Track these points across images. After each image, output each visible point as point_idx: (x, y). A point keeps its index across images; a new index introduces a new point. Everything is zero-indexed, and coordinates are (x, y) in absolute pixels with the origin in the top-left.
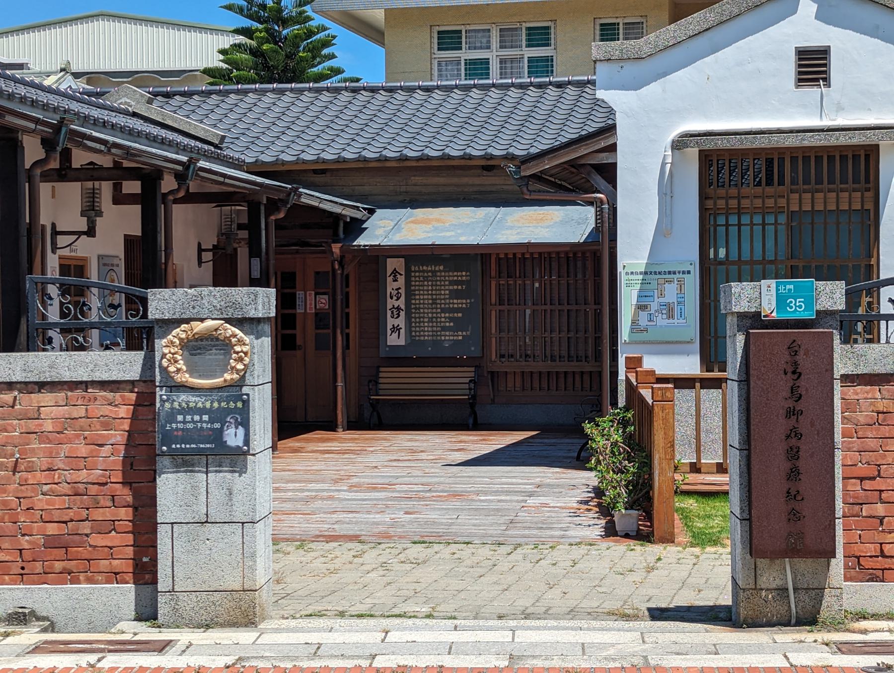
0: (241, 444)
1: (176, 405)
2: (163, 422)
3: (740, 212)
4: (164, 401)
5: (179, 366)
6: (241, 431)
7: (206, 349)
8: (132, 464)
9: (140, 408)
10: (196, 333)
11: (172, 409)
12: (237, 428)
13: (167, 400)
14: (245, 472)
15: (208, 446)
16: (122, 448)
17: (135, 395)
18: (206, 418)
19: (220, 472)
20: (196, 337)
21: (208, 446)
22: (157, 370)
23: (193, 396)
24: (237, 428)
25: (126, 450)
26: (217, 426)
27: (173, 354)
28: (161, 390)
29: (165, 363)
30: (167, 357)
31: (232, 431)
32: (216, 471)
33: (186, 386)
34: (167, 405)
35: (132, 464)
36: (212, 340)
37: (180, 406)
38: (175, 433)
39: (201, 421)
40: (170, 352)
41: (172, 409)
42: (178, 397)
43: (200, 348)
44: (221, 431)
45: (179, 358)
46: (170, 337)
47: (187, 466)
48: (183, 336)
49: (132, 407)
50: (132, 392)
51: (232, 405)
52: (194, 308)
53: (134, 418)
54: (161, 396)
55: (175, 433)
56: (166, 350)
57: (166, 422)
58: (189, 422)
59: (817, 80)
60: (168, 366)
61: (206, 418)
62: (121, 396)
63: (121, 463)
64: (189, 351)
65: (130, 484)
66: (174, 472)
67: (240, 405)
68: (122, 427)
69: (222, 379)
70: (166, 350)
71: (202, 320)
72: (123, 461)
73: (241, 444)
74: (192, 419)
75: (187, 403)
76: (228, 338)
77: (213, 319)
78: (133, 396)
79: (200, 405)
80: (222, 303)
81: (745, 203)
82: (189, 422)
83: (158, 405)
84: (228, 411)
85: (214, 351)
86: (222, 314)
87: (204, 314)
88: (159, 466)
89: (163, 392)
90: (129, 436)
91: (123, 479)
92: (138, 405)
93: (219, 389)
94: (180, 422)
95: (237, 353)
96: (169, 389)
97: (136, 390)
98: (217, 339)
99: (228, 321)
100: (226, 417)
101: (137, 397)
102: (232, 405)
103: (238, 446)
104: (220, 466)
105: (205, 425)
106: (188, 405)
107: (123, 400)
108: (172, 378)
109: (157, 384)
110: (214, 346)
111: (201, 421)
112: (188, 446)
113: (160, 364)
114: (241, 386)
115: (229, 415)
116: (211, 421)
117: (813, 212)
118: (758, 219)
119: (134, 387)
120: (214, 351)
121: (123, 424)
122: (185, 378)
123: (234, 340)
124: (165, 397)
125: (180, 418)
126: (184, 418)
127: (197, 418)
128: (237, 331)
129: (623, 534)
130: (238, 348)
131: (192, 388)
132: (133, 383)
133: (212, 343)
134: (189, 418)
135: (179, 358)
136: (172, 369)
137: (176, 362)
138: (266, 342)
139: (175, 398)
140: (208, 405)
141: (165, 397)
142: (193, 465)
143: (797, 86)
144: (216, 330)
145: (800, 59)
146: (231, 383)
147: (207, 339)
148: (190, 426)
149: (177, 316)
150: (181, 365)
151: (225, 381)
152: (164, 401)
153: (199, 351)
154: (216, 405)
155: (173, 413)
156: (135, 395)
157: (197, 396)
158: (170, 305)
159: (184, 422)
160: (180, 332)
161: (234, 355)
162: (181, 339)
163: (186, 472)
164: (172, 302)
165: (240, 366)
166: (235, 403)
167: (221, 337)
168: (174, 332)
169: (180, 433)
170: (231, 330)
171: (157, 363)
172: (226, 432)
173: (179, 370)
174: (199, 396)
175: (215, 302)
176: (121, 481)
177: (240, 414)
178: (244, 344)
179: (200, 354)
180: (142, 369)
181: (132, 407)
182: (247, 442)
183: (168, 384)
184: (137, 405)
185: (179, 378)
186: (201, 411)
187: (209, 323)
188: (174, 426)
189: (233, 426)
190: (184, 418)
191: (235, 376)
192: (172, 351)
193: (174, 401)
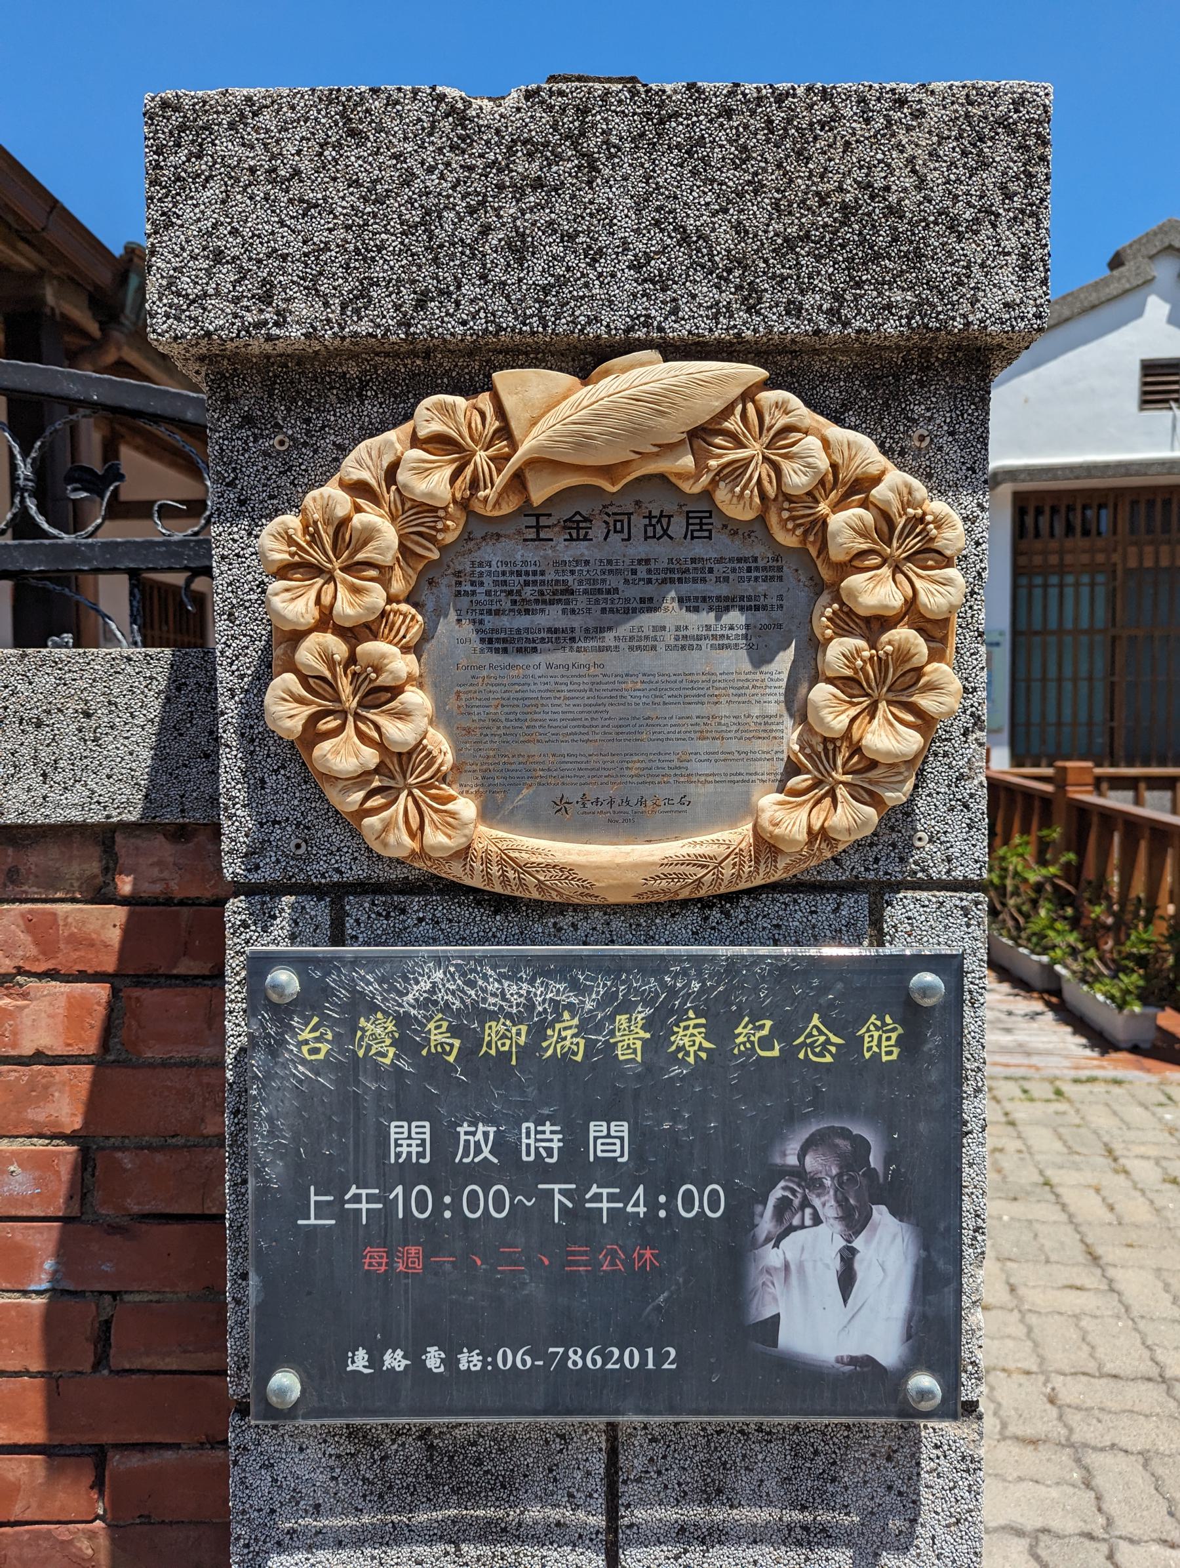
0: (887, 1347)
1: (377, 1036)
2: (275, 1172)
3: (1061, 570)
4: (282, 1012)
5: (399, 732)
6: (888, 1248)
7: (616, 600)
8: (103, 1336)
9: (150, 996)
10: (540, 463)
11: (348, 1067)
12: (855, 1221)
13: (311, 1000)
14: (904, 1543)
15: (631, 1358)
16: (42, 1241)
17: (119, 914)
18: (609, 1139)
19: (712, 1536)
20: (540, 491)
21: (631, 1358)
22: (230, 761)
23: (513, 968)
24: (855, 1221)
25: (64, 1252)
26: (701, 1202)
27: (353, 634)
28: (265, 919)
29: (286, 710)
30: (307, 654)
31: (816, 1245)
32: (683, 1534)
33: (454, 890)
34: (310, 1042)
35: (103, 1336)
36: (657, 527)
37: (402, 1044)
38: (374, 1259)
39: (575, 1163)
40: (326, 621)
41: (348, 1067)
42: (396, 976)
43: (562, 594)
44: (725, 1259)
45: (402, 665)
46: (329, 497)
47: (463, 1493)
48: (434, 482)
49: (100, 992)
50: (101, 895)
51: (819, 1040)
52: (519, 249)
53: (115, 1052)
54: (260, 965)
55: (374, 1259)
56: (294, 604)
57: (301, 1173)
58: (482, 1174)
59: (1166, 401)
60: (312, 735)
61: (609, 1139)
62: (30, 924)
63: (35, 1333)
64: (477, 614)
65: (99, 1455)
66: (359, 1539)
67: (881, 1040)
68: (38, 1115)
69: (739, 835)
70: (294, 604)
71: (586, 359)
72: (51, 1319)
73: (887, 1347)
74: (506, 1147)
75: (468, 1022)
76: (804, 513)
77: (672, 351)
78: (107, 924)
79: (565, 1038)
80: (757, 213)
81: (1069, 559)
82: (482, 1174)
83: (236, 1029)
84: (789, 1091)
85: (671, 615)
86: (752, 301)
87: (612, 305)
88: (249, 1490)
89: (276, 938)
90: (85, 1163)
91: (53, 1421)
92: (140, 980)
93: (708, 906)
94: (409, 1173)
95: (874, 625)
96: (320, 911)
97: (125, 885)
98: (703, 516)
99: (786, 364)
100: (773, 1135)
101: (129, 932)
102: (819, 1040)
103: (866, 1365)
104: (713, 1493)
105: (602, 1199)
106: (472, 1043)
107: (46, 946)
108: (350, 824)
109: (232, 868)
110: (674, 574)
111: (575, 1163)
112: (470, 1361)
113: (254, 713)
114: (881, 892)
115: (792, 1118)
116: (655, 1166)
117: (1157, 569)
118: (1085, 579)
119: (111, 869)
120: (671, 615)
121: (42, 1093)
122: (461, 827)
123: (845, 523)
124: (286, 979)
125: (409, 1139)
126: (444, 1140)
127: (541, 1139)
128: (864, 450)
129: (1129, 1045)
130: (876, 591)
131: (500, 904)
132: (104, 838)
133: (661, 551)
134: (477, 1139)
135: (402, 665)
136: (344, 754)
137: (381, 695)
138: (743, 653)
139: (372, 988)
140: (630, 1037)
141: (286, 979)
142: (505, 1487)
143: (1141, 409)
144: (701, 436)
145: (1146, 375)
146: (806, 868)
147: (619, 524)
148: (489, 1203)
149: (377, 321)
150: (415, 721)
151: (766, 846)
152: (282, 1012)
153: (553, 616)
154: (690, 1037)
155: (347, 1116)
156: (119, 914)
157: (543, 969)
158: (319, 229)
159: (443, 1171)
160: (406, 458)
161: (840, 651)
162: (416, 514)
163: (451, 1535)
164: (343, 199)
165: (889, 737)
166: (846, 1025)
167: (737, 506)
168: (362, 461)
169: (411, 1258)
170: (824, 443)
171: (230, 708)
172: (772, 1257)
173: (397, 766)
174: (562, 969)
175: (696, 207)
176: (37, 1435)
177: (886, 1117)
178: (930, 555)
179: (560, 638)
180: (160, 754)
181: (100, 992)
182: (937, 1329)
183: (320, 870)
184: (128, 978)
185: (392, 829)
186: (585, 1088)
187: (642, 376)
188: (362, 1201)
189: (827, 1205)
190: (444, 1140)
191: (850, 816)
192: (347, 607)
193: (360, 1005)
